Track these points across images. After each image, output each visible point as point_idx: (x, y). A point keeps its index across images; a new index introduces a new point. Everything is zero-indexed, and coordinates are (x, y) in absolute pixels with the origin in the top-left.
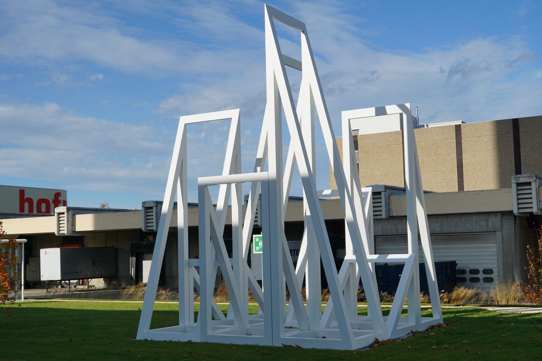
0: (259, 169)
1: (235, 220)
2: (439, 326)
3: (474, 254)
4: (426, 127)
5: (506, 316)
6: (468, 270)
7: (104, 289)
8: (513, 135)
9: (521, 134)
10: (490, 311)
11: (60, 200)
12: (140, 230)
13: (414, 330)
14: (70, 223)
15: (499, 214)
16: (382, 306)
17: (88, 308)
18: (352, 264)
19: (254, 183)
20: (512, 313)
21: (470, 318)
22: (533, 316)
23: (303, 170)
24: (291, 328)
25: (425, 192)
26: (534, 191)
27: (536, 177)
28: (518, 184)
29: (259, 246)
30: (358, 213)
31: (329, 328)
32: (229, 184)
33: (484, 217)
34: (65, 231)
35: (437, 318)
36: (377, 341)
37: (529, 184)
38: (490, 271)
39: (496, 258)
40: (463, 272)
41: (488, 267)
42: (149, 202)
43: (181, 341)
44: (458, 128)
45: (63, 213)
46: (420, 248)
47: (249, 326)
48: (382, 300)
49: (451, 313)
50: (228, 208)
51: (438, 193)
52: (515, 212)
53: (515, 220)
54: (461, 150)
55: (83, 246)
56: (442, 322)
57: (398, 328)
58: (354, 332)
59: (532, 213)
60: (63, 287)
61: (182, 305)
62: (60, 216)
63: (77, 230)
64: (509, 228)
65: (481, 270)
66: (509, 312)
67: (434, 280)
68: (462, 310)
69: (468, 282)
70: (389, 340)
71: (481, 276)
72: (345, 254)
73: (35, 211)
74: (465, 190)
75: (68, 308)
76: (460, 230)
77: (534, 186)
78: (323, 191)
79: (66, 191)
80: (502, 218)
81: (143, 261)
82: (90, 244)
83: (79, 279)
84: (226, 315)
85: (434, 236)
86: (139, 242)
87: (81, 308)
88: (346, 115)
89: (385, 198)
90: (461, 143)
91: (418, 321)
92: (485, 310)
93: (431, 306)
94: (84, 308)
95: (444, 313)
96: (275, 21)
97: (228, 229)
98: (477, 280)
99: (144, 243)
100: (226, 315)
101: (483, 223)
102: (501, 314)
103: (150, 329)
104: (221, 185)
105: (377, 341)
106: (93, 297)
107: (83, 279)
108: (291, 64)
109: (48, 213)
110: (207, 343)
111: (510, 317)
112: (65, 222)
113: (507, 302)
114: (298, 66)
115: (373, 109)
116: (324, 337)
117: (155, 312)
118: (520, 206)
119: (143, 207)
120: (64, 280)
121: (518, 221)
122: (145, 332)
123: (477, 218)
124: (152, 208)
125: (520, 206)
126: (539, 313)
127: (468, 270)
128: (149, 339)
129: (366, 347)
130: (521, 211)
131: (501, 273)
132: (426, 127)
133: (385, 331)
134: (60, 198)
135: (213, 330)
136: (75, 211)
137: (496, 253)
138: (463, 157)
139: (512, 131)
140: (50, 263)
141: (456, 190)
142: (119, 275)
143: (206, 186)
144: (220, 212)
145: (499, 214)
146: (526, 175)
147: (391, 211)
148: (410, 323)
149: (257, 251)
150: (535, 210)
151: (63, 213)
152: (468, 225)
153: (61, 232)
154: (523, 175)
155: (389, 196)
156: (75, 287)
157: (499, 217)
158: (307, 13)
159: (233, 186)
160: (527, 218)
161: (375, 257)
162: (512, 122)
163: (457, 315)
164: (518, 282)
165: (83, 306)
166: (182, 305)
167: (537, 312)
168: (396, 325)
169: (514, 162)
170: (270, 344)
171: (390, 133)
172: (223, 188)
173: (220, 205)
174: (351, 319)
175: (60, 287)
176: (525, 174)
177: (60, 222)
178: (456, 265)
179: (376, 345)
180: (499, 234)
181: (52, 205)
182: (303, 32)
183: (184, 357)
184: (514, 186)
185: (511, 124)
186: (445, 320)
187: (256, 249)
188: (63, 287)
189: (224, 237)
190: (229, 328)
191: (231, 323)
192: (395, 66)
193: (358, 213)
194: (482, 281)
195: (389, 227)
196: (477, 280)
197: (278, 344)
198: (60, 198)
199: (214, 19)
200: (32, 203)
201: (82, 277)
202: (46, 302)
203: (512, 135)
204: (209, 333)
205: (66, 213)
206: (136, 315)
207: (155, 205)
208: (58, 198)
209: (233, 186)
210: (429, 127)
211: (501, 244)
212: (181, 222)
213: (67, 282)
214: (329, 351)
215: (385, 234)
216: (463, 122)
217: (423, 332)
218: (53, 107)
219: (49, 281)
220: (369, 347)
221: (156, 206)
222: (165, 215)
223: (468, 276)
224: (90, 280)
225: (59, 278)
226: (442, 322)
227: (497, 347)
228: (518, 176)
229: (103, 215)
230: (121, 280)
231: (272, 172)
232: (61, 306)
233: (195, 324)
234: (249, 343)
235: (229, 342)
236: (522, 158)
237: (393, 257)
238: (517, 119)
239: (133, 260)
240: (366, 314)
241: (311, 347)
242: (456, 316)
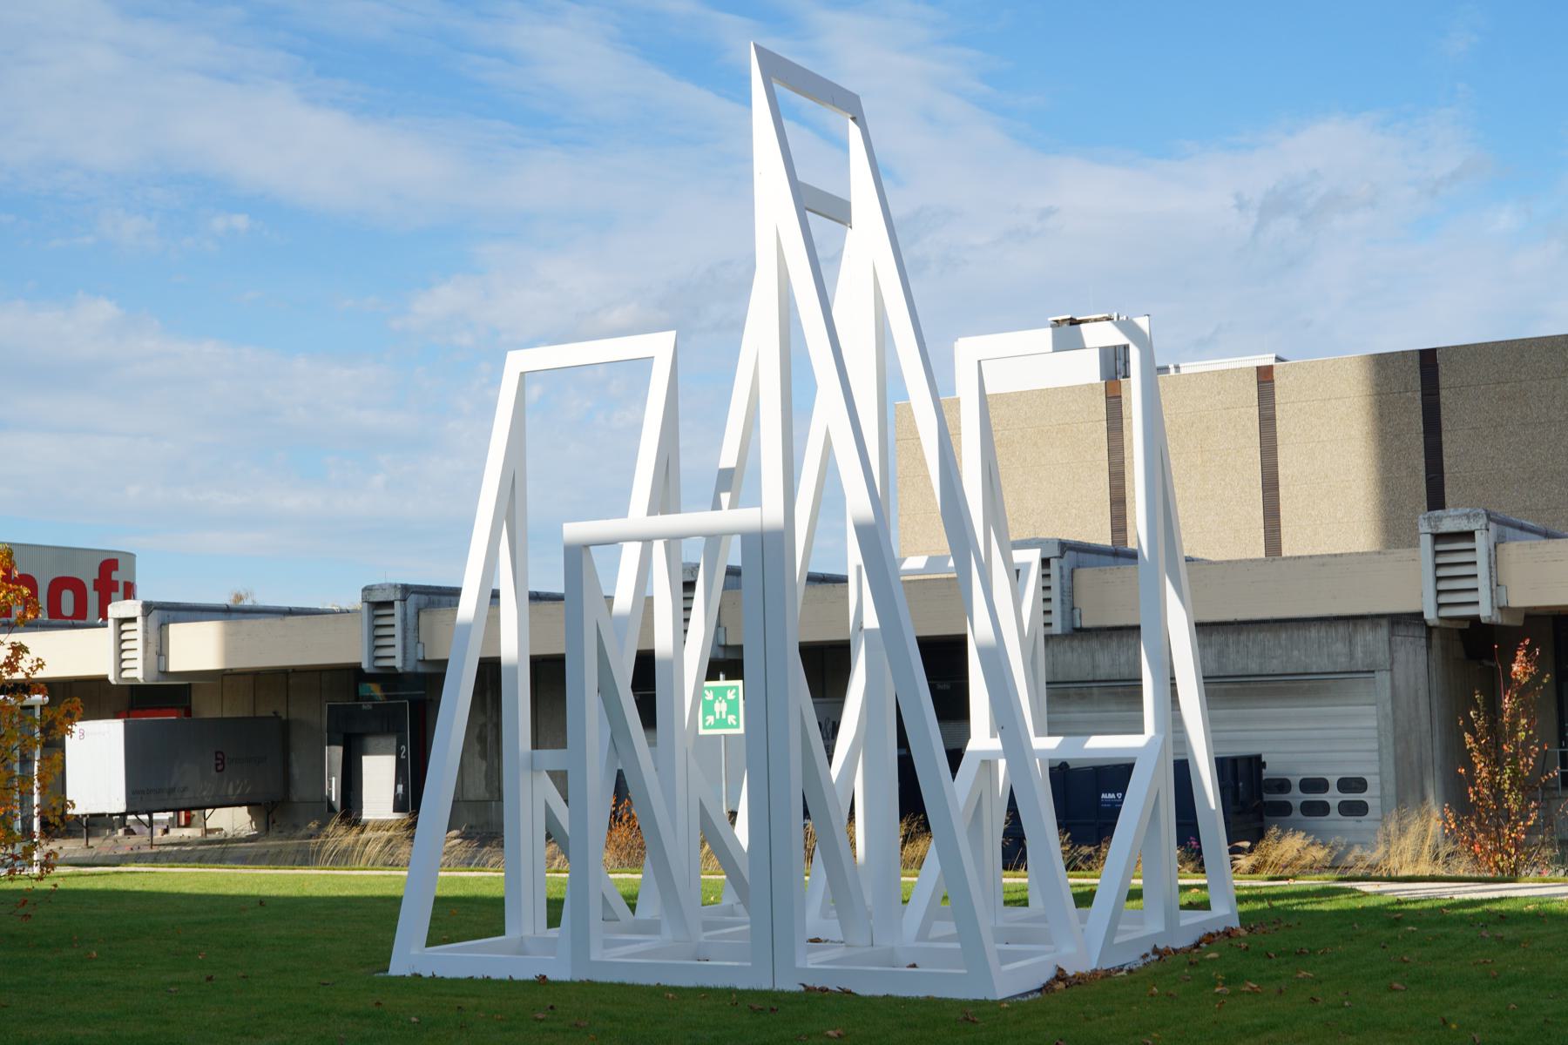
0: (725, 497)
1: (663, 644)
2: (1229, 933)
3: (1316, 733)
4: (1172, 371)
5: (1412, 906)
6: (1295, 781)
7: (249, 839)
8: (1423, 394)
9: (1443, 393)
10: (1366, 894)
11: (116, 583)
13: (1161, 946)
14: (153, 648)
15: (1384, 622)
16: (1071, 881)
17: (233, 891)
18: (988, 764)
19: (714, 540)
20: (1428, 899)
21: (1312, 911)
22: (1486, 907)
23: (858, 504)
24: (817, 940)
25: (1188, 560)
26: (1481, 557)
27: (1488, 516)
28: (1438, 538)
29: (714, 714)
30: (1002, 620)
32: (647, 541)
33: (1342, 629)
34: (137, 672)
35: (1223, 913)
36: (1060, 976)
37: (1469, 535)
38: (1359, 784)
39: (1376, 746)
40: (1283, 785)
41: (1352, 771)
42: (382, 588)
43: (516, 978)
44: (1265, 376)
45: (133, 620)
46: (1175, 721)
47: (703, 937)
48: (1071, 866)
49: (1259, 898)
50: (645, 604)
51: (1210, 563)
52: (1430, 615)
53: (1429, 638)
54: (1275, 438)
55: (188, 712)
56: (1236, 924)
57: (1117, 940)
58: (999, 951)
59: (1475, 620)
60: (129, 832)
61: (513, 879)
62: (124, 627)
63: (171, 669)
64: (1412, 662)
65: (1333, 781)
66: (1420, 895)
67: (1213, 806)
68: (1289, 890)
69: (1297, 814)
70: (1095, 972)
71: (1333, 797)
72: (968, 736)
73: (43, 616)
74: (1286, 552)
75: (174, 889)
76: (1275, 666)
77: (1481, 542)
78: (904, 560)
79: (133, 555)
80: (1392, 634)
82: (207, 708)
83: (177, 810)
84: (633, 907)
85: (1217, 686)
86: (384, 698)
87: (212, 891)
88: (968, 350)
89: (1062, 576)
90: (1273, 418)
91: (1170, 921)
92: (1352, 890)
93: (1204, 882)
94: (221, 891)
95: (1241, 900)
96: (777, 87)
97: (645, 664)
98: (1323, 809)
100: (633, 907)
101: (1340, 647)
102: (1399, 902)
103: (428, 945)
104: (627, 546)
105: (1060, 976)
106: (213, 856)
107: (187, 810)
108: (820, 207)
109: (79, 619)
110: (590, 983)
111: (1423, 909)
112: (139, 645)
113: (1412, 863)
114: (839, 212)
115: (1047, 334)
116: (914, 966)
117: (439, 901)
118: (1444, 599)
119: (364, 601)
120: (136, 813)
121: (1436, 641)
122: (412, 954)
123: (1323, 633)
124: (390, 604)
125: (1444, 599)
126: (1501, 899)
127: (1295, 781)
128: (426, 974)
129: (1031, 992)
130: (1445, 612)
131: (1391, 789)
132: (1172, 371)
133: (1082, 946)
134: (115, 576)
135: (605, 947)
136: (165, 614)
137: (1375, 733)
138: (1280, 459)
139: (1418, 385)
140: (96, 765)
142: (295, 799)
143: (586, 546)
144: (623, 620)
145: (1384, 622)
146: (1461, 511)
147: (1077, 612)
148: (1152, 927)
149: (710, 727)
150: (398, 663)
151: (133, 620)
152: (1296, 653)
153: (125, 675)
154: (1450, 511)
155: (1072, 572)
156: (166, 831)
157: (1383, 632)
158: (848, 50)
159: (659, 548)
160: (1461, 631)
161: (1052, 743)
162: (1417, 358)
163: (1276, 903)
164: (1436, 813)
165: (217, 886)
166: (513, 879)
167: (1496, 895)
168: (1112, 930)
169: (1423, 473)
170: (766, 986)
171: (1072, 389)
172: (631, 554)
173: (624, 600)
174: (991, 919)
175: (121, 832)
176: (1456, 506)
177: (124, 646)
178: (1264, 765)
179: (1061, 985)
180: (1383, 678)
181: (93, 597)
182: (853, 119)
183: (536, 1019)
184: (1426, 541)
185: (1415, 364)
186: (1243, 917)
187: (705, 721)
188: (129, 832)
189: (635, 687)
190: (648, 942)
191: (651, 928)
192: (1097, 199)
193: (1002, 620)
194: (1334, 813)
195: (1090, 661)
196: (1323, 809)
197: (790, 984)
198: (115, 576)
199: (573, 57)
200: (85, 590)
201: (187, 805)
202: (107, 874)
203: (1419, 395)
204: (596, 955)
205: (140, 620)
206: (385, 911)
207: (399, 596)
208: (110, 578)
209: (659, 548)
210: (1183, 371)
211: (1389, 708)
212: (512, 649)
213: (145, 817)
214: (930, 1002)
215: (1060, 678)
216: (1278, 359)
217: (1187, 951)
218: (104, 310)
219: (92, 816)
220: (1039, 990)
221: (404, 600)
222: (467, 627)
223: (1296, 797)
224: (208, 812)
225: (122, 809)
226: (1236, 924)
227: (1392, 989)
228: (1438, 513)
229: (248, 624)
230: (294, 812)
231: (769, 512)
232: (152, 885)
233: (554, 933)
234: (710, 982)
235: (651, 980)
236: (1446, 462)
237: (1103, 745)
238: (1434, 351)
239: (334, 754)
240: (1024, 903)
241: (881, 993)
242: (1272, 908)
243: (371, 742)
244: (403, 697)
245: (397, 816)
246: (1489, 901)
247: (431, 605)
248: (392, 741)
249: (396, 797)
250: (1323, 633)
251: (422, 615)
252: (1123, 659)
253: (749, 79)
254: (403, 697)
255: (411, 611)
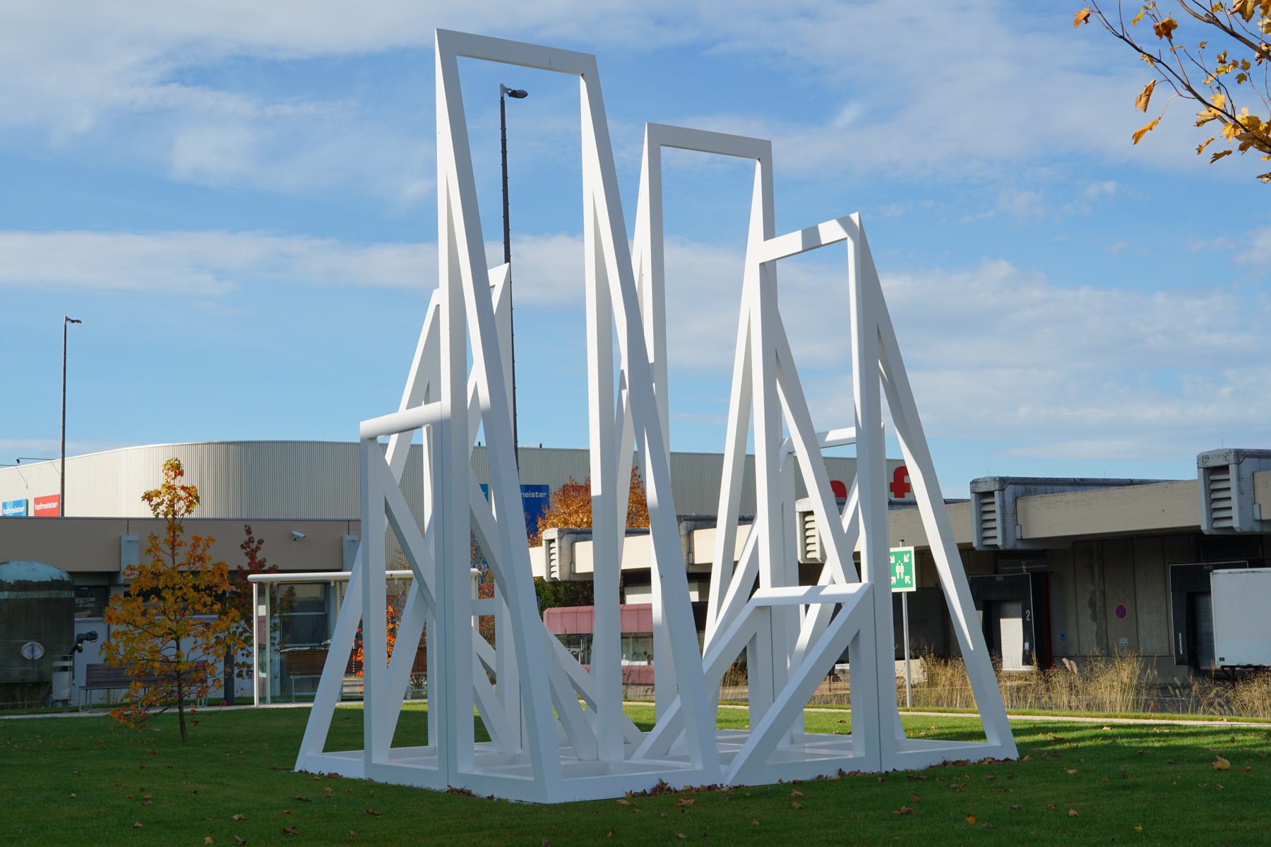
12: (1194, 532)
25: (947, 502)
31: (666, 755)
42: (985, 481)
48: (423, 715)
56: (1014, 755)
81: (1002, 621)
95: (1016, 732)
99: (999, 578)
124: (991, 494)
141: (946, 496)
150: (999, 542)
153: (809, 556)
186: (1021, 747)
226: (1014, 755)
243: (1009, 607)
245: (1027, 668)
246: (1073, 740)
247: (1028, 493)
248: (1018, 607)
249: (1024, 652)
251: (1019, 503)
253: (754, 172)
255: (1009, 498)
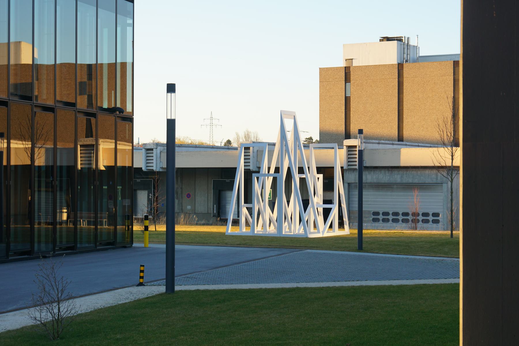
41: (436, 211)
124: (152, 149)
150: (154, 168)
185: (86, 69)
244: (151, 178)
250: (408, 172)
252: (375, 177)
254: (151, 178)
255: (159, 152)
